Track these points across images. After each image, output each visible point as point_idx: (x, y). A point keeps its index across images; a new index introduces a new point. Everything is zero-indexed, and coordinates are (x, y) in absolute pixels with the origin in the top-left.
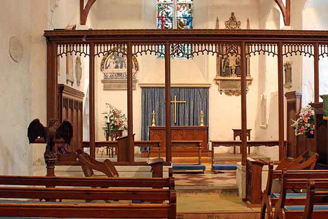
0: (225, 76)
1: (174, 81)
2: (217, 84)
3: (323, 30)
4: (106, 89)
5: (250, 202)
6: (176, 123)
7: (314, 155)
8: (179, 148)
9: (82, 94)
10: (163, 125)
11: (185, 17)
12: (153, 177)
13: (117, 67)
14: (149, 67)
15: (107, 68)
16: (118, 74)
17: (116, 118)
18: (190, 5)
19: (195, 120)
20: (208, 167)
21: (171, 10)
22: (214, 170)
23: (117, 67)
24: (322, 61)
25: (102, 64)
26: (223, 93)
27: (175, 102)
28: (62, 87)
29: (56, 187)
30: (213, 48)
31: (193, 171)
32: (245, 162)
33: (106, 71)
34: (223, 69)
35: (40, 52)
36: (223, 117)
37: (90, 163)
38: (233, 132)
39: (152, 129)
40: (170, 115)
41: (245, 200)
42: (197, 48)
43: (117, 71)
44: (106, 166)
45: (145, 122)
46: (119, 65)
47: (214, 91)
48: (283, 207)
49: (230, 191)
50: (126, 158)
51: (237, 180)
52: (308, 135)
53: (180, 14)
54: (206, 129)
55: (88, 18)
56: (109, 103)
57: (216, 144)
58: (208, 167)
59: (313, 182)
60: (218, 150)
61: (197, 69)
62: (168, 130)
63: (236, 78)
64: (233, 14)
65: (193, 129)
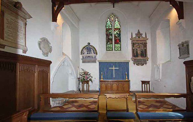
0: (136, 57)
2: (132, 60)
3: (131, 85)
4: (83, 62)
11: (117, 33)
13: (88, 53)
15: (83, 54)
16: (88, 56)
17: (85, 75)
18: (119, 29)
23: (88, 53)
25: (81, 52)
26: (135, 64)
27: (114, 68)
33: (83, 55)
38: (184, 66)
40: (69, 25)
46: (89, 53)
47: (131, 63)
56: (83, 68)
64: (139, 30)
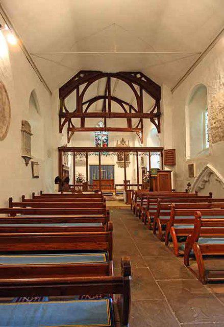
1: (102, 163)
5: (191, 249)
6: (103, 178)
7: (149, 188)
8: (103, 187)
9: (69, 168)
10: (98, 179)
12: (10, 207)
14: (93, 159)
19: (110, 177)
20: (114, 194)
21: (100, 137)
22: (117, 194)
24: (151, 157)
28: (63, 166)
29: (13, 207)
30: (116, 153)
31: (110, 194)
32: (126, 191)
34: (120, 159)
35: (57, 154)
36: (119, 178)
37: (73, 190)
39: (94, 180)
41: (126, 203)
42: (110, 153)
43: (80, 159)
44: (79, 191)
45: (91, 178)
47: (116, 167)
48: (159, 217)
49: (122, 200)
50: (86, 190)
51: (124, 197)
52: (148, 182)
53: (103, 138)
54: (113, 180)
55: (63, 129)
57: (117, 185)
58: (114, 194)
59: (159, 200)
60: (118, 188)
61: (110, 159)
62: (100, 180)
63: (124, 162)
65: (108, 180)
